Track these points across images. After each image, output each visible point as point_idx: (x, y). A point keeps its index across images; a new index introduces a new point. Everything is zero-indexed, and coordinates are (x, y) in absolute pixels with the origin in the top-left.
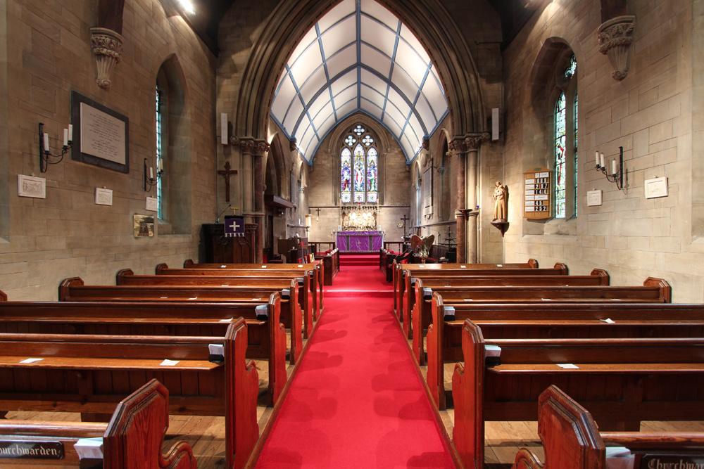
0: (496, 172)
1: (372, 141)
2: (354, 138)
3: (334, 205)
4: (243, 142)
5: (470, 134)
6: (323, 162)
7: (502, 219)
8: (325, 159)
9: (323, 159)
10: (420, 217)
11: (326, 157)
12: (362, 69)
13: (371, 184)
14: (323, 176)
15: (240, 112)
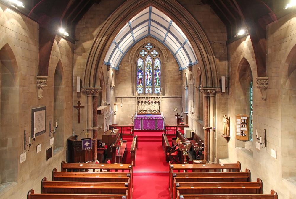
0: (224, 109)
1: (157, 53)
2: (145, 51)
3: (132, 96)
4: (88, 90)
5: (211, 88)
6: (125, 68)
7: (227, 134)
8: (127, 66)
9: (125, 66)
10: (187, 107)
11: (128, 64)
12: (151, 22)
13: (156, 81)
14: (125, 76)
15: (87, 74)
